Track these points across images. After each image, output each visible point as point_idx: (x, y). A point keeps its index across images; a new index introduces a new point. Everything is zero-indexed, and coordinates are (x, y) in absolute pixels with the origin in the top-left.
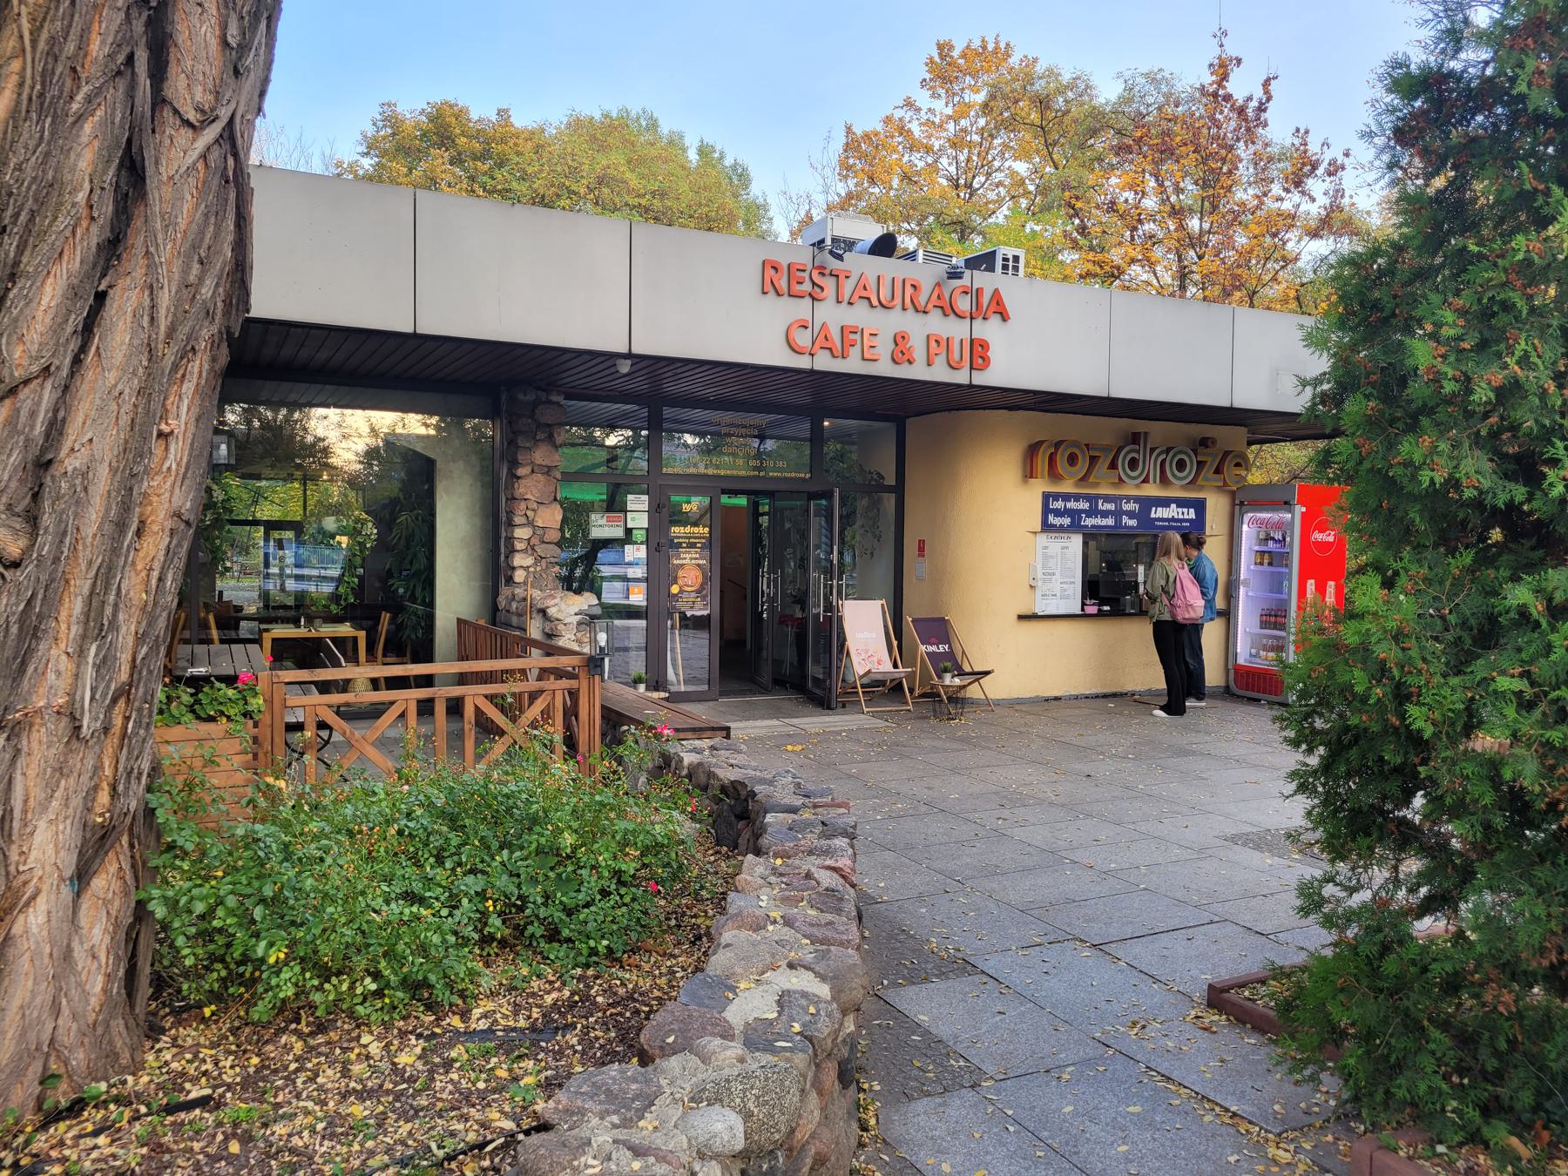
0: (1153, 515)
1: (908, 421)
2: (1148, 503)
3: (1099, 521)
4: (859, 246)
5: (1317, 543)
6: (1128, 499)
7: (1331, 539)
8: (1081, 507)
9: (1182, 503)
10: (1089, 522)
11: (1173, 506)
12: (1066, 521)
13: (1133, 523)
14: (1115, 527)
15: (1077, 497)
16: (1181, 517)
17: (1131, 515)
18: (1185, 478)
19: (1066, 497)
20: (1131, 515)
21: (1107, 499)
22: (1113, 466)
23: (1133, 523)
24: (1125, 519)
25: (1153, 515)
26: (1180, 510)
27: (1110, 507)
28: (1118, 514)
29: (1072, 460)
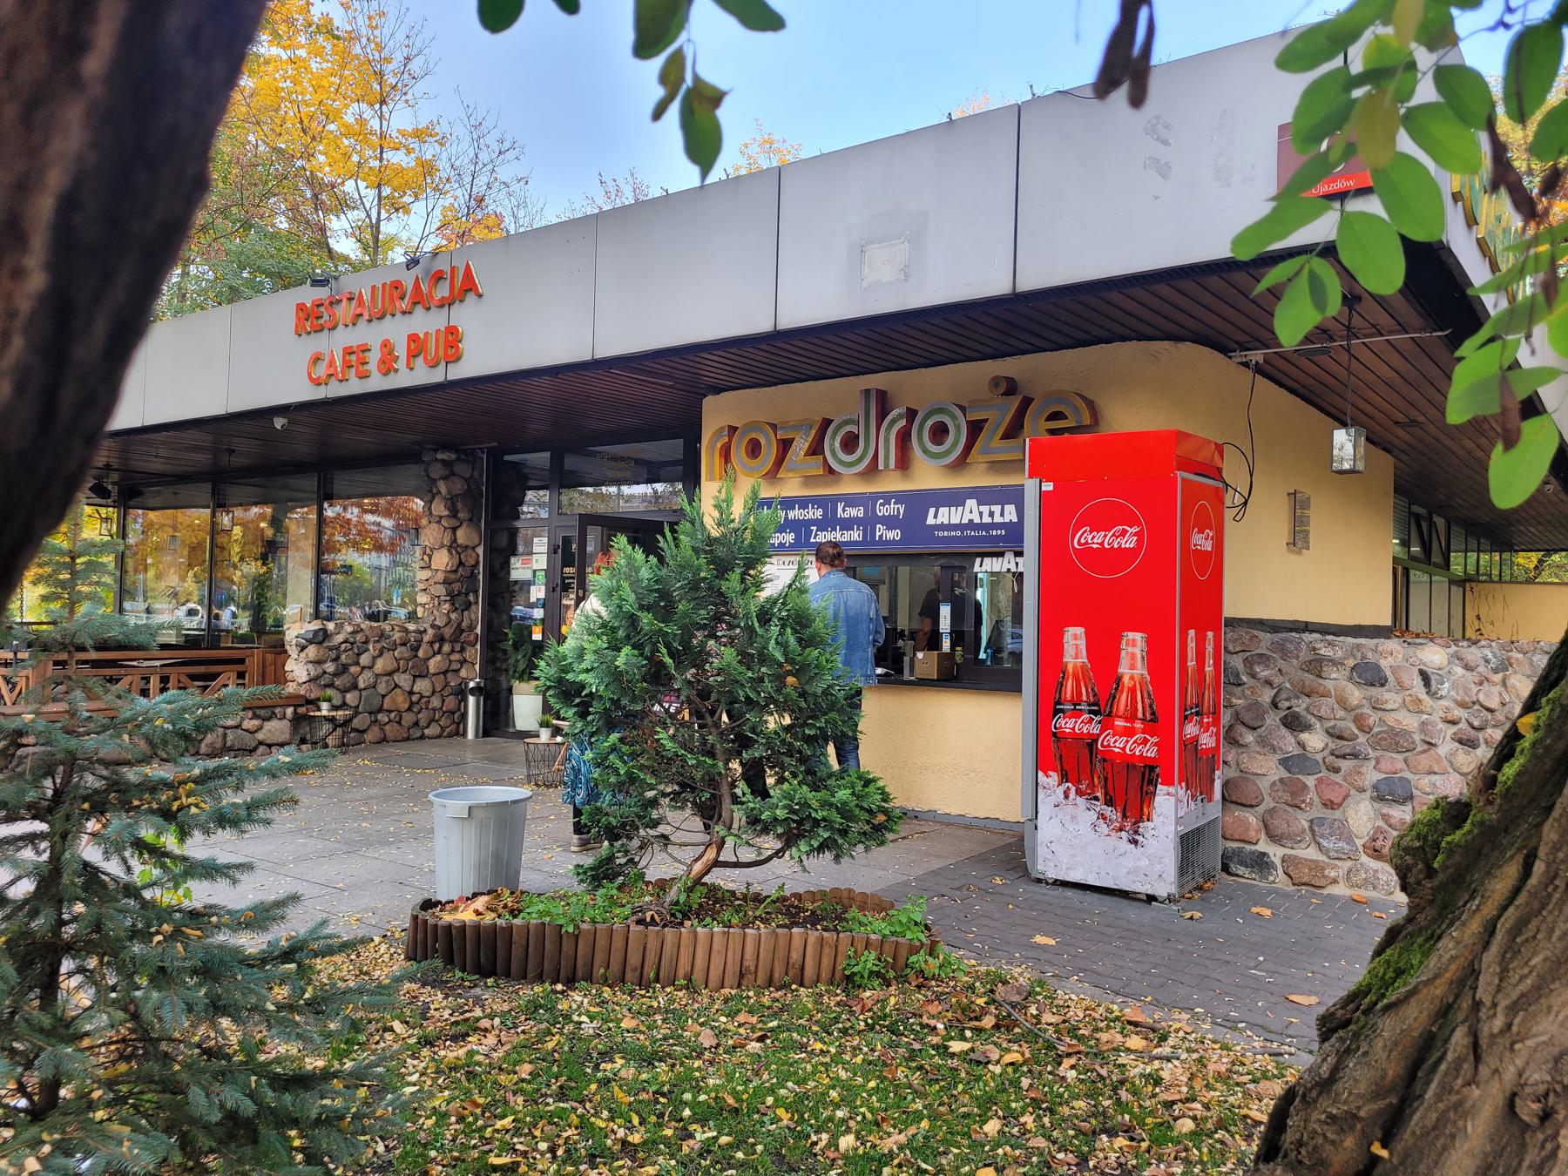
0: (930, 521)
1: (705, 401)
2: (920, 502)
3: (838, 536)
4: (1400, 69)
5: (1086, 553)
6: (887, 497)
7: (1129, 542)
8: (810, 516)
9: (985, 496)
10: (823, 537)
11: (971, 503)
12: (789, 538)
13: (893, 535)
14: (864, 542)
15: (803, 503)
16: (987, 519)
17: (890, 522)
18: (948, 452)
19: (788, 503)
20: (890, 522)
21: (851, 501)
22: (816, 449)
23: (893, 535)
24: (880, 530)
25: (930, 521)
26: (985, 509)
27: (857, 512)
28: (868, 523)
29: (754, 449)
